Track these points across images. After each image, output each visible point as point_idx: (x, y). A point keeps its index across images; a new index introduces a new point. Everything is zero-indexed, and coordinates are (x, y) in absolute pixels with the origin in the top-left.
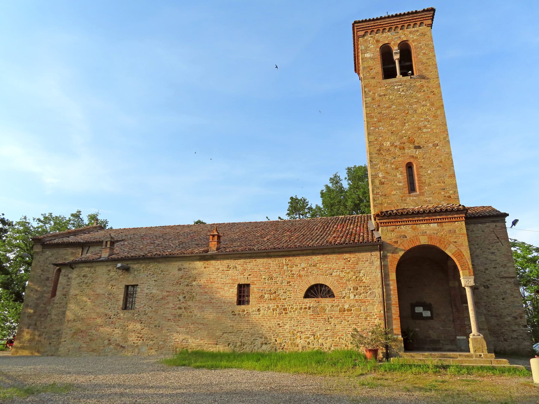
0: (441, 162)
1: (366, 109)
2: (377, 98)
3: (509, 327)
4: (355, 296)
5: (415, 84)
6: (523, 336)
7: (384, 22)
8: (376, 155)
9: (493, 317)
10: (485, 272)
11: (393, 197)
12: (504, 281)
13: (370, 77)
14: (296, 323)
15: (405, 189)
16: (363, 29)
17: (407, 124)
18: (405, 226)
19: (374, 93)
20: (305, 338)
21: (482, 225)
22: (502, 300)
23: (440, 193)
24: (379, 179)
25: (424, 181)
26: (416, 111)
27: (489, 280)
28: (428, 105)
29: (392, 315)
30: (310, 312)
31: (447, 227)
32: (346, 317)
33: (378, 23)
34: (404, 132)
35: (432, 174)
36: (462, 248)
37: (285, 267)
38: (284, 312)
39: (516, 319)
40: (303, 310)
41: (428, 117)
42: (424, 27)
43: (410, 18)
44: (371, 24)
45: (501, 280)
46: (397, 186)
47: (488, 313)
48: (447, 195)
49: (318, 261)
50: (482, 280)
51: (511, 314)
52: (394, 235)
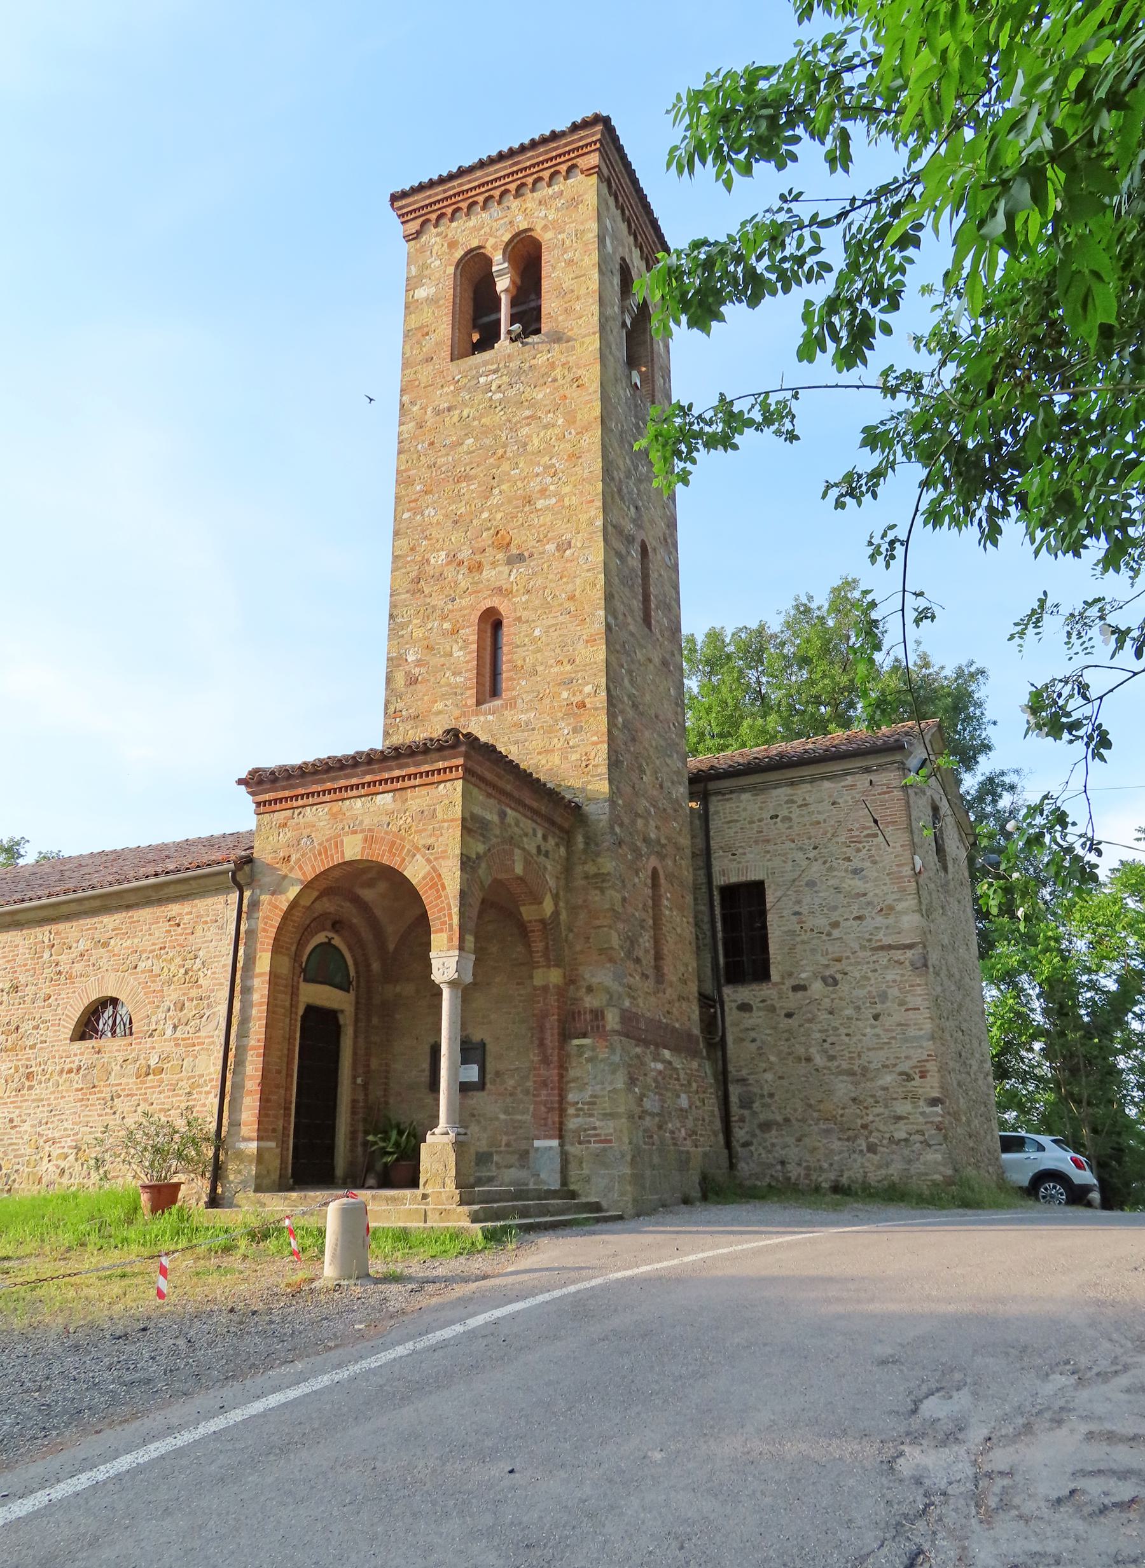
0: (572, 598)
1: (398, 459)
2: (430, 418)
3: (886, 1107)
4: (175, 1027)
5: (533, 362)
6: (923, 1135)
7: (470, 182)
8: (408, 595)
9: (841, 1078)
10: (829, 934)
11: (435, 719)
12: (883, 958)
13: (420, 357)
14: (46, 1114)
15: (469, 693)
16: (418, 214)
17: (496, 491)
18: (315, 807)
19: (424, 408)
20: (58, 1157)
21: (833, 785)
22: (872, 1021)
23: (555, 696)
24: (407, 668)
25: (520, 663)
26: (525, 445)
27: (839, 960)
28: (560, 422)
29: (243, 1080)
30: (77, 1080)
31: (419, 799)
32: (149, 1091)
33: (454, 187)
34: (485, 515)
35: (544, 639)
36: (443, 863)
37: (46, 955)
38: (27, 1084)
39: (907, 1080)
40: (64, 1076)
41: (554, 461)
42: (581, 177)
43: (541, 159)
44: (436, 194)
45: (874, 958)
46: (449, 685)
47: (829, 1064)
48: (578, 698)
49: (113, 930)
50: (821, 958)
51: (895, 1065)
52: (287, 835)
